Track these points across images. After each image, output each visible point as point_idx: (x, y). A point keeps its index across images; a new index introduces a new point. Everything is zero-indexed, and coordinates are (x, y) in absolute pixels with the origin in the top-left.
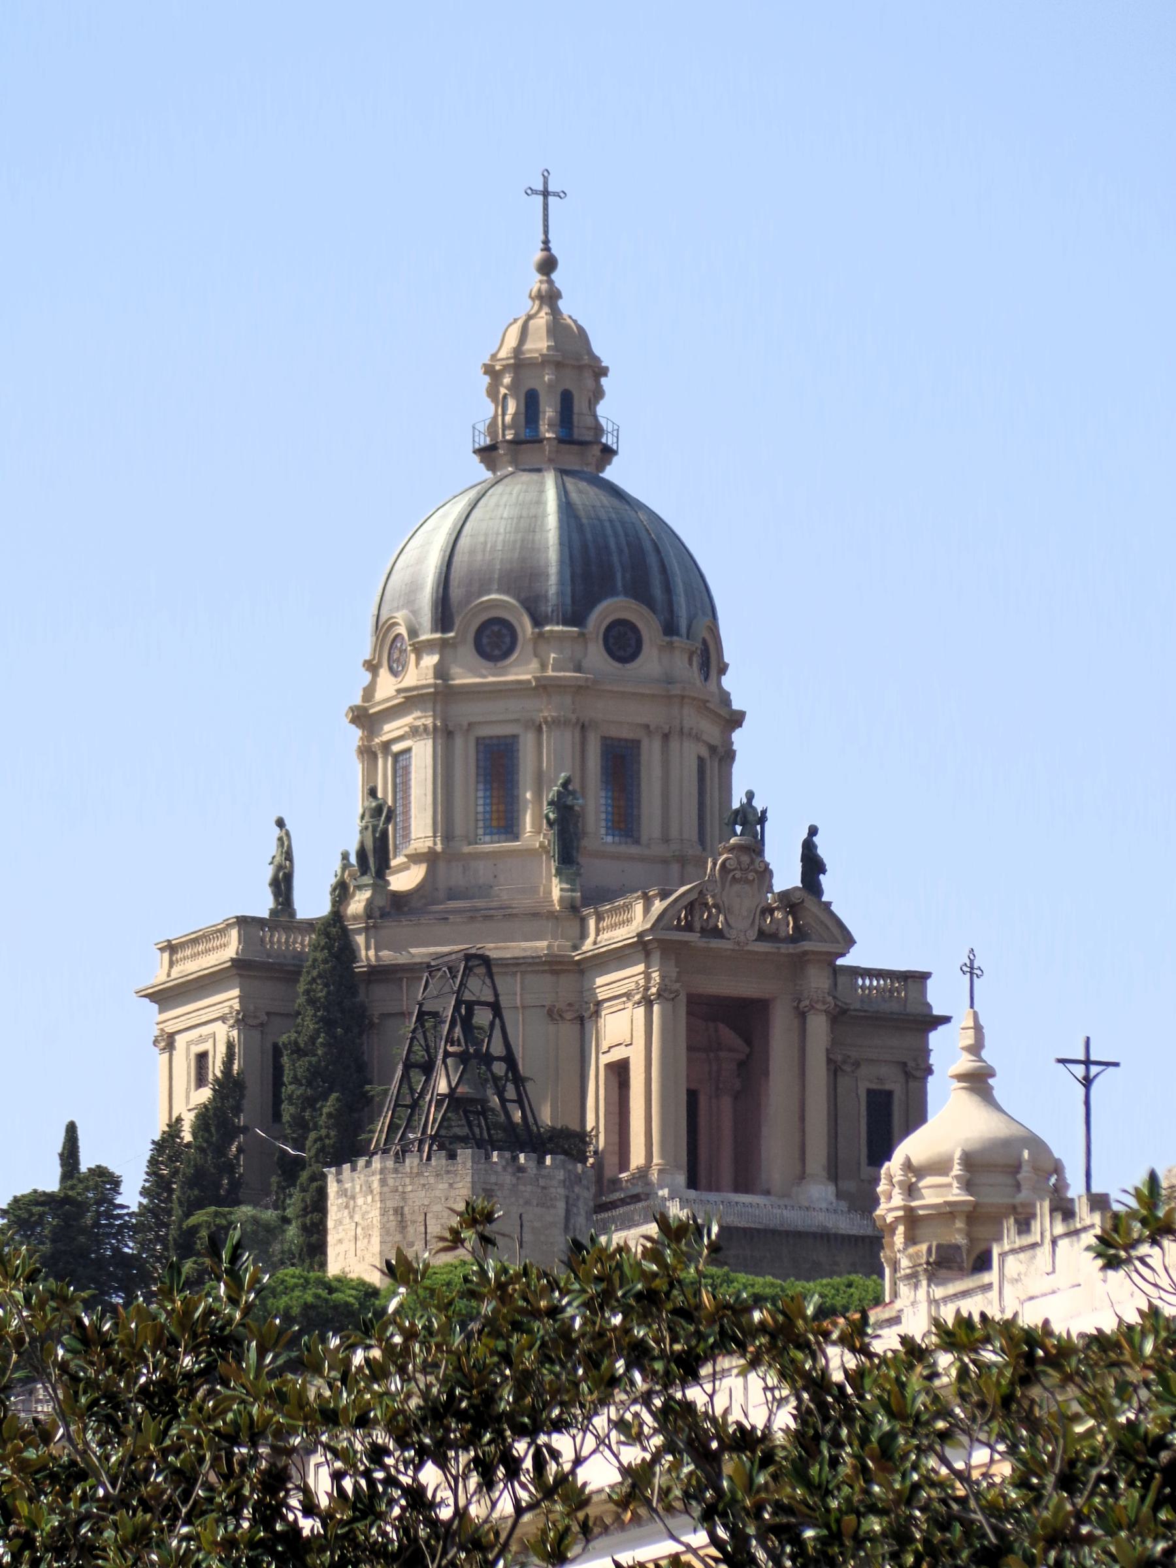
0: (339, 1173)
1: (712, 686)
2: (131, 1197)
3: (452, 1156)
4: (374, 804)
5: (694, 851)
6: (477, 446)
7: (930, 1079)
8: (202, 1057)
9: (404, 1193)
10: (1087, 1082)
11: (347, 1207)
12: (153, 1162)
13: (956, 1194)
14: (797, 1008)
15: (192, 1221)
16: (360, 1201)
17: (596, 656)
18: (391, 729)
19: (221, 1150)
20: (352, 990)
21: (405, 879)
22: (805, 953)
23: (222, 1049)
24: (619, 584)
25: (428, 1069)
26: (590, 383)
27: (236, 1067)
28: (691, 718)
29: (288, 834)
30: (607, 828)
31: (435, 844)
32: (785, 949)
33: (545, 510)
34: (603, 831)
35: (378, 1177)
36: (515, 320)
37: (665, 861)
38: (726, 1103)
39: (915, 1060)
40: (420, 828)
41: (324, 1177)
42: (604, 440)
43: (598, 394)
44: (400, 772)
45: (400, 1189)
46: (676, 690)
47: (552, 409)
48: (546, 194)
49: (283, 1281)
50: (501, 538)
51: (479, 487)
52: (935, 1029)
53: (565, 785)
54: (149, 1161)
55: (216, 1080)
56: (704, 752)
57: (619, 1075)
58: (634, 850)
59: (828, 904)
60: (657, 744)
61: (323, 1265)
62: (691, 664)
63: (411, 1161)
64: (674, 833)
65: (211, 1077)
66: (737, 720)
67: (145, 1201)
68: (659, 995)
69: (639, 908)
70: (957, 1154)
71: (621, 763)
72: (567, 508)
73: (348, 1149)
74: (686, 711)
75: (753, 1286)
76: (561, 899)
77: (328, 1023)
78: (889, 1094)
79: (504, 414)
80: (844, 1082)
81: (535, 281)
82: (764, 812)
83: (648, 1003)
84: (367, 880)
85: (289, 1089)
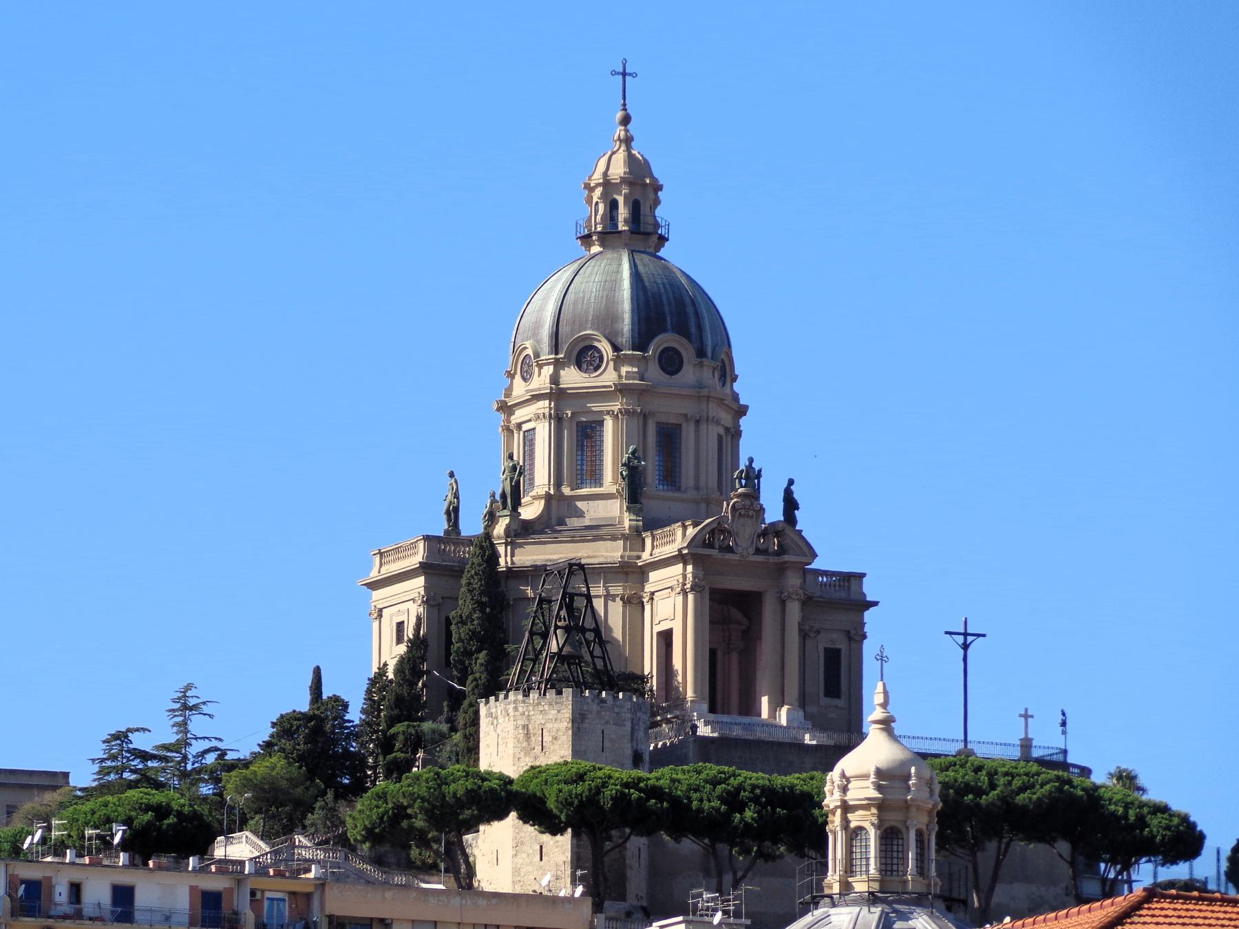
0: (487, 702)
1: (728, 391)
2: (355, 715)
3: (559, 693)
5: (716, 495)
8: (400, 625)
10: (965, 647)
12: (369, 692)
15: (392, 731)
16: (501, 721)
17: (654, 371)
18: (519, 415)
21: (530, 510)
22: (785, 562)
23: (413, 620)
25: (545, 636)
26: (652, 196)
28: (714, 411)
32: (772, 559)
37: (697, 502)
38: (735, 657)
43: (657, 202)
46: (705, 392)
47: (633, 215)
48: (624, 74)
53: (633, 453)
55: (409, 640)
56: (722, 431)
58: (676, 495)
60: (692, 427)
61: (477, 760)
63: (534, 695)
64: (702, 483)
66: (742, 411)
68: (692, 589)
69: (679, 532)
70: (872, 771)
71: (669, 439)
72: (636, 276)
73: (493, 688)
74: (711, 405)
76: (630, 527)
77: (481, 605)
80: (810, 644)
81: (620, 131)
83: (685, 593)
84: (506, 512)
85: (454, 648)
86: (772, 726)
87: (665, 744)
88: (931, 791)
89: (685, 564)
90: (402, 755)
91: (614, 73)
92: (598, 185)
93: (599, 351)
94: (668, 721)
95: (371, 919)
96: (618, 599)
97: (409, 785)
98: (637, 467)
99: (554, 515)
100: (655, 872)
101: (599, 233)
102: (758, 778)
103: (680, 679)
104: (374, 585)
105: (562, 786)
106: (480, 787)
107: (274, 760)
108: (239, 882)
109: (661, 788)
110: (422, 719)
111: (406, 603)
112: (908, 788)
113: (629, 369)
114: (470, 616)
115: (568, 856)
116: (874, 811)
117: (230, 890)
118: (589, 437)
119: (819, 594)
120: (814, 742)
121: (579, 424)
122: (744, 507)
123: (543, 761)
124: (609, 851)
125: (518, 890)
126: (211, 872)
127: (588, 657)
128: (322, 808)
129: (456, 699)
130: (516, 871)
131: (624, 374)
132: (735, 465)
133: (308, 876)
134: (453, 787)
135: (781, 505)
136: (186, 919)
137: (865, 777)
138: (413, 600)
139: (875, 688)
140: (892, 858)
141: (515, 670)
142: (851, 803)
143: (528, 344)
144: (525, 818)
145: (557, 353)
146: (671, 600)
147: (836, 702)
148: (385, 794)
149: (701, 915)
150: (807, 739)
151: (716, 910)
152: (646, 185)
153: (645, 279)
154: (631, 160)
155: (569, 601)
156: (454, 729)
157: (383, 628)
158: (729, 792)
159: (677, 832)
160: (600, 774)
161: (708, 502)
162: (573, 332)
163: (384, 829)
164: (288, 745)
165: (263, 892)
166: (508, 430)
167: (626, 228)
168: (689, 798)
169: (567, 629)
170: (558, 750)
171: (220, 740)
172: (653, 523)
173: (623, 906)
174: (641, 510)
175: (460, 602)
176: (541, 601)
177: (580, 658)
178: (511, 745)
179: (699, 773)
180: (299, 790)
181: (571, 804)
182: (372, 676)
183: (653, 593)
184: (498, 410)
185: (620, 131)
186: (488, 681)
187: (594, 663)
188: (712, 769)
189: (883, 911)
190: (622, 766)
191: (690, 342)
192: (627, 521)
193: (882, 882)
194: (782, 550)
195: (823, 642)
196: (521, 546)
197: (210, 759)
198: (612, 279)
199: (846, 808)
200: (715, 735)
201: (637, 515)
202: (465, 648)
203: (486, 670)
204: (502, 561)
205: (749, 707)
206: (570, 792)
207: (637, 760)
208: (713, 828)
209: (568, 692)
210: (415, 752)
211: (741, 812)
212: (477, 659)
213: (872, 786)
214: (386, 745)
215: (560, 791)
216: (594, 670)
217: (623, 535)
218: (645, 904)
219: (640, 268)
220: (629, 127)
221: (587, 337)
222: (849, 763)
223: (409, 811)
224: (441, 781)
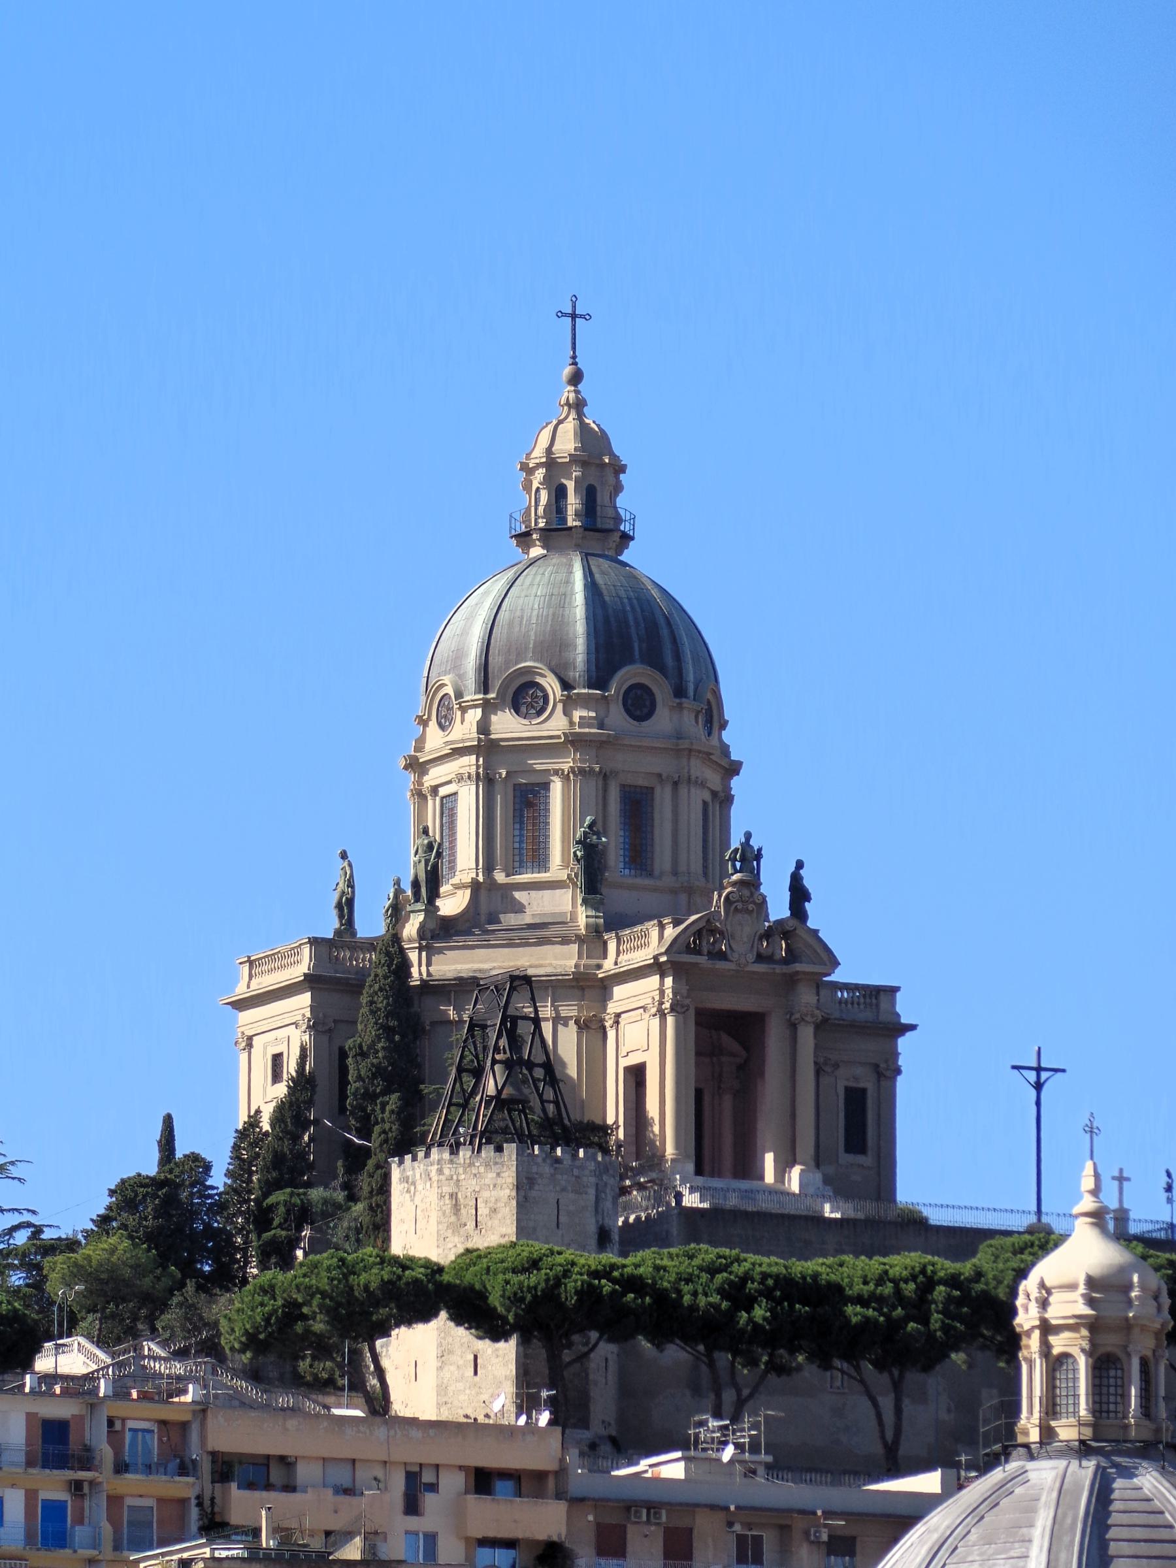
0: (401, 1162)
1: (714, 741)
2: (218, 1180)
3: (499, 1149)
4: (426, 842)
5: (700, 882)
6: (513, 533)
7: (899, 1078)
8: (277, 1059)
9: (458, 1181)
10: (1038, 1086)
11: (408, 1191)
12: (236, 1148)
14: (789, 1020)
15: (271, 1200)
16: (420, 1187)
17: (618, 716)
18: (435, 775)
19: (296, 1138)
20: (408, 1002)
21: (452, 904)
22: (797, 973)
23: (295, 1053)
24: (637, 653)
25: (478, 1073)
26: (611, 479)
27: (307, 1067)
28: (698, 769)
29: (350, 865)
30: (625, 863)
31: (477, 875)
32: (778, 969)
33: (572, 589)
34: (621, 865)
35: (436, 1167)
36: (547, 424)
37: (674, 892)
38: (727, 1102)
39: (886, 1061)
41: (389, 1165)
42: (622, 528)
43: (618, 488)
44: (446, 812)
45: (455, 1177)
46: (684, 744)
47: (586, 509)
48: (574, 316)
49: (363, 1260)
50: (535, 613)
51: (515, 568)
52: (903, 1034)
53: (590, 826)
54: (233, 1147)
55: (292, 1079)
56: (707, 796)
57: (637, 1076)
58: (647, 882)
59: (816, 932)
60: (668, 790)
61: (387, 1240)
62: (697, 722)
63: (465, 1153)
64: (682, 868)
65: (285, 1076)
66: (734, 769)
67: (229, 1182)
68: (672, 1009)
69: (654, 933)
71: (637, 807)
72: (592, 589)
73: (406, 1143)
74: (693, 762)
75: (760, 1265)
76: (587, 926)
77: (388, 1031)
79: (537, 505)
80: (825, 1080)
81: (568, 393)
82: (760, 850)
83: (662, 1015)
84: (420, 906)
85: (351, 1089)
86: (778, 1192)
87: (638, 1218)
88: (1159, 1309)
89: (663, 977)
90: (284, 1233)
91: (561, 314)
92: (539, 465)
93: (543, 690)
94: (641, 1187)
95: (268, 1457)
96: (571, 1023)
97: (305, 1276)
98: (596, 846)
99: (484, 909)
100: (626, 1391)
101: (541, 529)
102: (771, 1263)
103: (656, 1129)
104: (241, 1005)
105: (509, 1276)
106: (400, 1278)
107: (113, 1240)
108: (92, 1407)
109: (640, 1277)
110: (309, 1185)
111: (286, 1028)
112: (1129, 1302)
113: (584, 713)
114: (372, 1046)
115: (511, 1369)
116: (1085, 1332)
117: (81, 1418)
118: (530, 805)
119: (837, 1015)
120: (838, 1216)
121: (517, 787)
122: (741, 899)
123: (482, 1242)
124: (570, 1363)
125: (445, 1416)
126: (54, 1395)
127: (535, 1102)
128: (180, 1305)
129: (356, 1159)
130: (442, 1389)
131: (576, 720)
132: (726, 842)
133: (183, 1399)
134: (363, 1278)
135: (787, 896)
136: (21, 1458)
137: (1072, 1287)
138: (296, 1024)
139: (1082, 1168)
140: (1108, 1394)
141: (436, 1121)
142: (1054, 1322)
143: (446, 679)
144: (458, 1318)
145: (486, 692)
146: (644, 1024)
147: (860, 1159)
148: (272, 1287)
149: (704, 1450)
150: (828, 1211)
151: (725, 1443)
152: (603, 465)
153: (605, 592)
154: (584, 431)
155: (510, 1024)
156: (352, 1198)
157: (249, 1065)
158: (731, 1283)
159: (659, 1337)
160: (560, 1259)
161: (690, 891)
162: (508, 664)
163: (270, 1335)
164: (132, 1221)
165: (123, 1420)
166: (420, 795)
167: (578, 523)
168: (679, 1292)
169: (508, 1065)
170: (498, 1229)
171: (34, 1212)
172: (617, 921)
173: (586, 1435)
174: (601, 902)
175: (360, 1027)
176: (472, 1027)
177: (525, 1102)
178: (433, 1220)
179: (691, 1257)
180: (147, 1281)
181: (522, 1299)
182: (240, 1127)
183: (618, 1015)
184: (406, 768)
185: (568, 393)
186: (402, 1133)
187: (544, 1110)
188: (708, 1253)
189: (1098, 1467)
190: (583, 1248)
191: (666, 677)
192: (583, 918)
193: (1095, 1426)
194: (792, 956)
195: (842, 1080)
196: (440, 951)
197: (21, 1238)
198: (561, 590)
199: (1046, 1328)
200: (706, 1205)
201: (597, 910)
202: (367, 1089)
203: (399, 1119)
204: (415, 971)
205: (748, 1167)
206: (521, 1283)
207: (603, 1238)
208: (710, 1331)
209: (511, 1149)
210: (299, 1229)
211: (749, 1310)
212: (384, 1106)
213: (1081, 1301)
214: (262, 1219)
215: (507, 1282)
216: (543, 1119)
217: (578, 937)
218: (614, 1433)
219: (597, 576)
220: (580, 387)
221: (528, 671)
223: (305, 1310)
224: (348, 1269)
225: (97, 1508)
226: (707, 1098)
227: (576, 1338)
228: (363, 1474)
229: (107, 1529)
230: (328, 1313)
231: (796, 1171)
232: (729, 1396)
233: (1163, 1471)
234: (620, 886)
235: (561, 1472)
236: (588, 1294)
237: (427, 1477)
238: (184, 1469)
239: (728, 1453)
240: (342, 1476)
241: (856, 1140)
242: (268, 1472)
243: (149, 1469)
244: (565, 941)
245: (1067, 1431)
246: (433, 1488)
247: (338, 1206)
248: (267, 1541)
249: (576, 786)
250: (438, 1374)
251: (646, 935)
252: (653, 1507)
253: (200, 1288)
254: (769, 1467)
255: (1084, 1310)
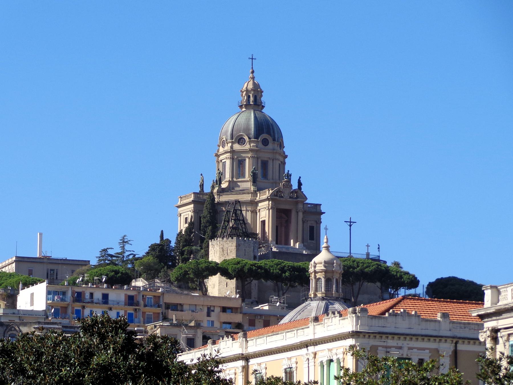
2: (173, 244)
3: (232, 238)
10: (350, 226)
12: (177, 238)
13: (323, 268)
15: (184, 249)
17: (260, 145)
18: (221, 157)
19: (190, 235)
21: (224, 185)
23: (190, 217)
25: (228, 222)
26: (260, 94)
28: (278, 156)
32: (294, 200)
37: (272, 183)
38: (283, 229)
40: (228, 176)
43: (262, 96)
46: (275, 151)
47: (255, 100)
48: (252, 59)
56: (280, 163)
58: (267, 181)
60: (271, 161)
63: (225, 239)
66: (286, 157)
68: (271, 208)
69: (267, 192)
70: (323, 261)
71: (265, 165)
72: (255, 117)
73: (213, 236)
77: (210, 213)
78: (313, 227)
81: (251, 75)
83: (269, 210)
85: (202, 225)
94: (264, 247)
99: (231, 186)
100: (260, 291)
109: (262, 266)
110: (192, 246)
111: (188, 212)
116: (323, 273)
123: (228, 258)
125: (220, 296)
129: (202, 240)
130: (219, 290)
137: (321, 263)
144: (222, 275)
147: (313, 241)
150: (304, 252)
154: (254, 83)
156: (202, 249)
160: (244, 262)
161: (276, 183)
162: (237, 134)
164: (153, 253)
166: (218, 162)
170: (232, 255)
172: (260, 189)
178: (218, 254)
179: (273, 262)
185: (251, 75)
188: (276, 261)
190: (250, 260)
193: (326, 294)
194: (297, 197)
195: (309, 224)
196: (222, 195)
198: (248, 118)
199: (315, 272)
204: (216, 200)
205: (287, 243)
208: (277, 278)
209: (235, 238)
214: (182, 253)
216: (242, 232)
222: (316, 259)
225: (140, 315)
226: (279, 228)
227: (248, 279)
228: (198, 308)
229: (142, 319)
230: (194, 273)
231: (297, 244)
232: (281, 293)
233: (340, 304)
234: (260, 182)
235: (241, 308)
236: (250, 270)
237: (212, 309)
238: (159, 306)
239: (278, 304)
240: (193, 308)
241: (312, 237)
242: (176, 307)
243: (151, 306)
244: (248, 193)
245: (319, 295)
246: (213, 311)
247: (198, 250)
248: (174, 322)
249: (251, 160)
250: (217, 286)
251: (266, 192)
252: (261, 315)
253: (167, 268)
254: (286, 307)
255: (323, 268)
